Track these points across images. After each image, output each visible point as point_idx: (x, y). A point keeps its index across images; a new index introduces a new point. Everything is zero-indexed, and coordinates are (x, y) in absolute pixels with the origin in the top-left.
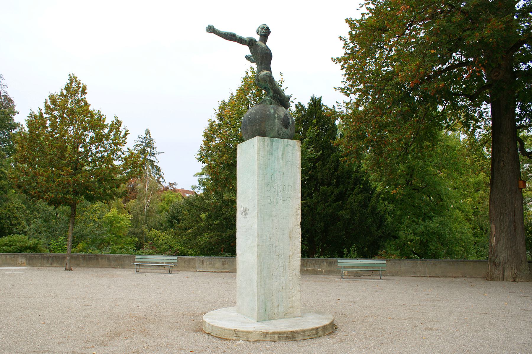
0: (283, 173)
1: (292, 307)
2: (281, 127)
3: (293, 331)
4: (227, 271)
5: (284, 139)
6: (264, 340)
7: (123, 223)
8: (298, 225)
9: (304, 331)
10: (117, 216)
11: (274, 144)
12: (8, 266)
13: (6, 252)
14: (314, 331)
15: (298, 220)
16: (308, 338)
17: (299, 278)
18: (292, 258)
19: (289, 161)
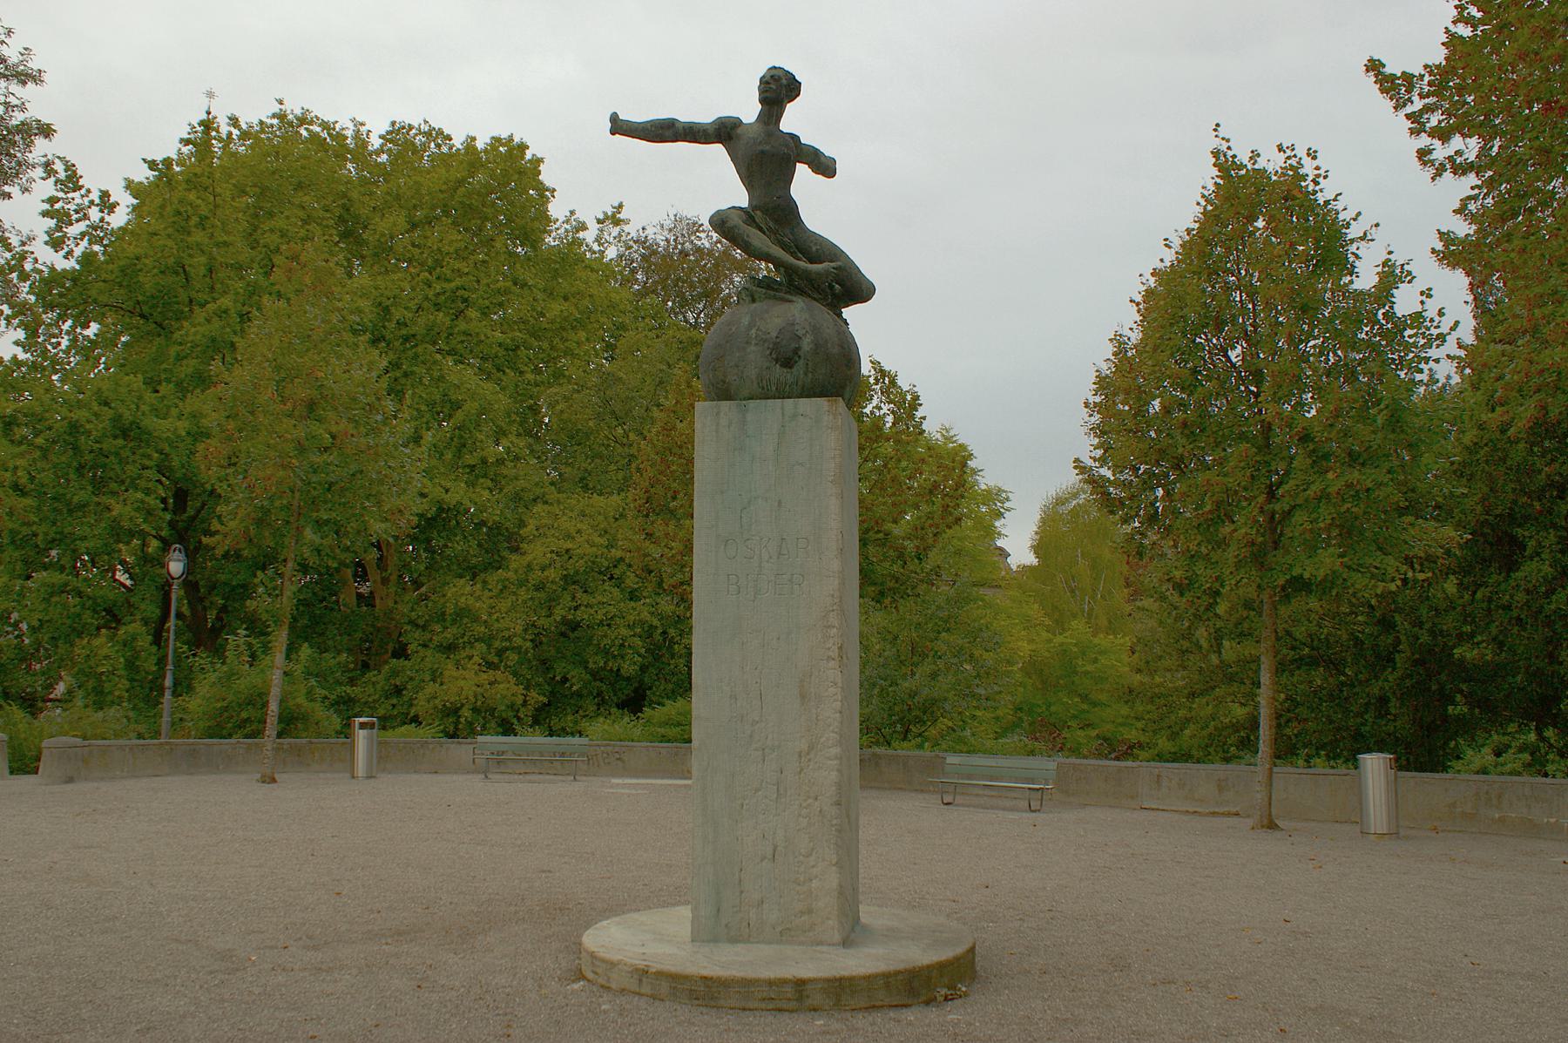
0: (780, 502)
1: (810, 911)
2: (768, 364)
3: (712, 978)
4: (1234, 810)
5: (783, 398)
6: (637, 990)
7: (1103, 660)
8: (830, 658)
9: (747, 983)
10: (1091, 642)
11: (749, 417)
12: (662, 778)
13: (669, 741)
14: (789, 991)
15: (831, 641)
16: (763, 1005)
17: (835, 822)
18: (809, 760)
19: (801, 464)
